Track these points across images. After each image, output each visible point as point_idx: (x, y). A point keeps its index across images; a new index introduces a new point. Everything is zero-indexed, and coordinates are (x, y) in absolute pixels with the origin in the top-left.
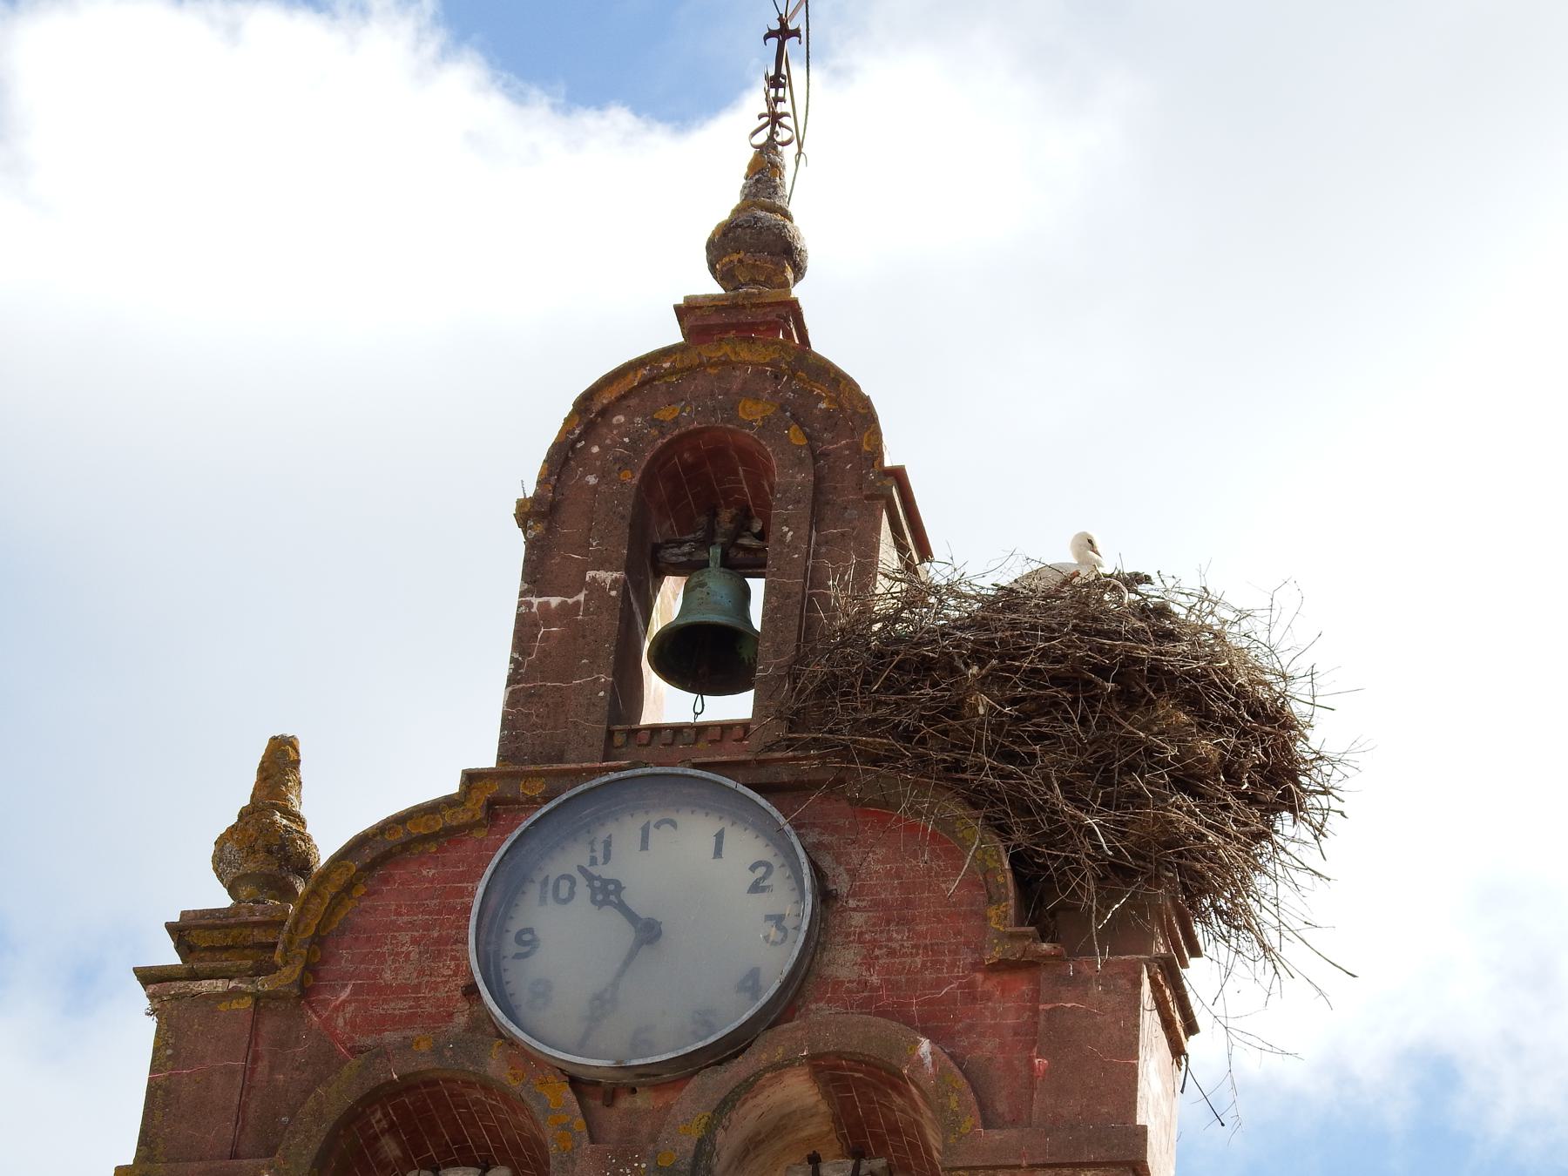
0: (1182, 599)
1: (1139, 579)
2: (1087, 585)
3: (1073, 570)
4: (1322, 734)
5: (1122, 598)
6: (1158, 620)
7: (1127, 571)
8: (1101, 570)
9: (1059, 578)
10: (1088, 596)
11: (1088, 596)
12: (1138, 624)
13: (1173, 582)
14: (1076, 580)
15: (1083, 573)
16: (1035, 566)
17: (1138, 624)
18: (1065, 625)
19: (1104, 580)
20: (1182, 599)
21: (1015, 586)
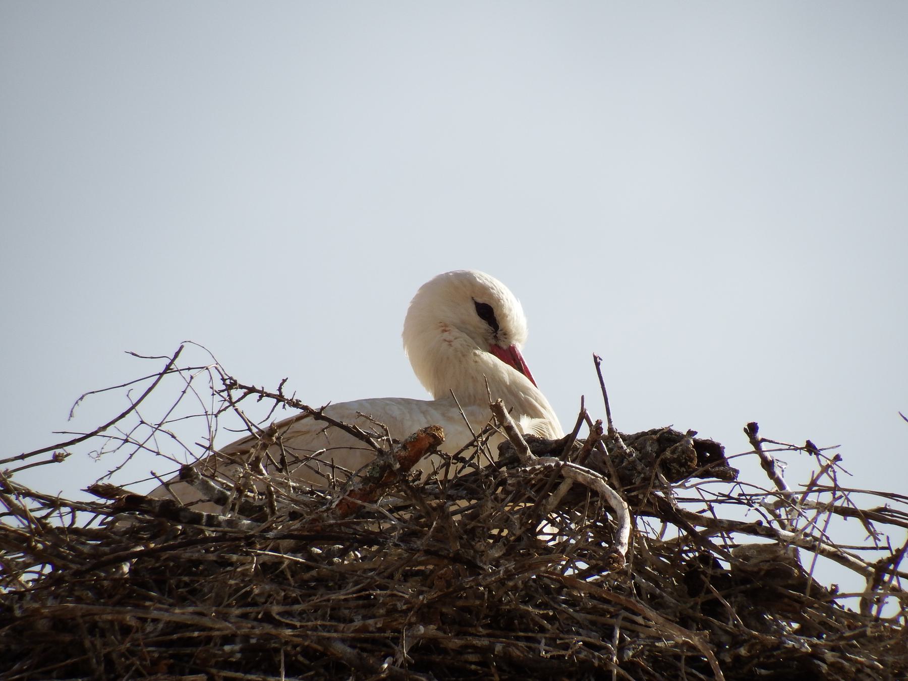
0: (846, 532)
1: (683, 455)
2: (472, 485)
3: (415, 426)
4: (716, 440)
5: (610, 533)
6: (754, 619)
7: (629, 423)
8: (526, 426)
9: (356, 461)
10: (473, 529)
11: (473, 529)
12: (677, 637)
13: (809, 465)
14: (426, 466)
15: (454, 437)
16: (262, 414)
17: (677, 637)
18: (382, 646)
19: (534, 464)
20: (846, 532)
21: (185, 495)
